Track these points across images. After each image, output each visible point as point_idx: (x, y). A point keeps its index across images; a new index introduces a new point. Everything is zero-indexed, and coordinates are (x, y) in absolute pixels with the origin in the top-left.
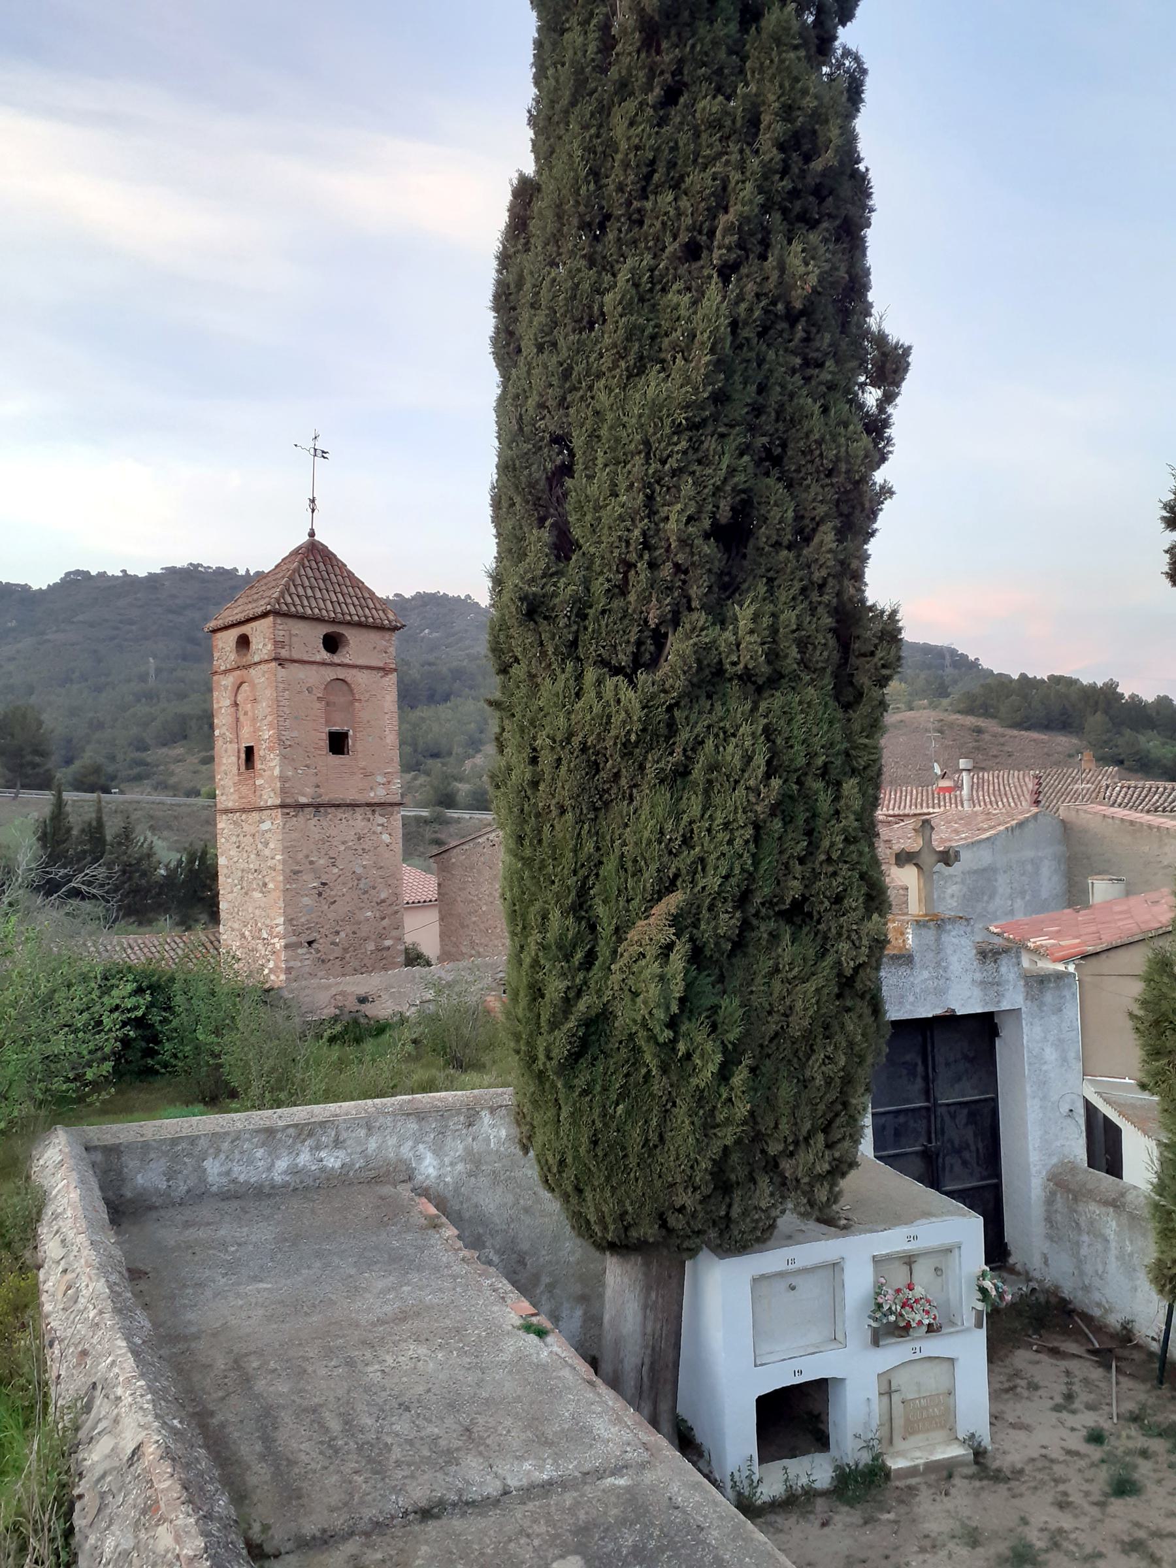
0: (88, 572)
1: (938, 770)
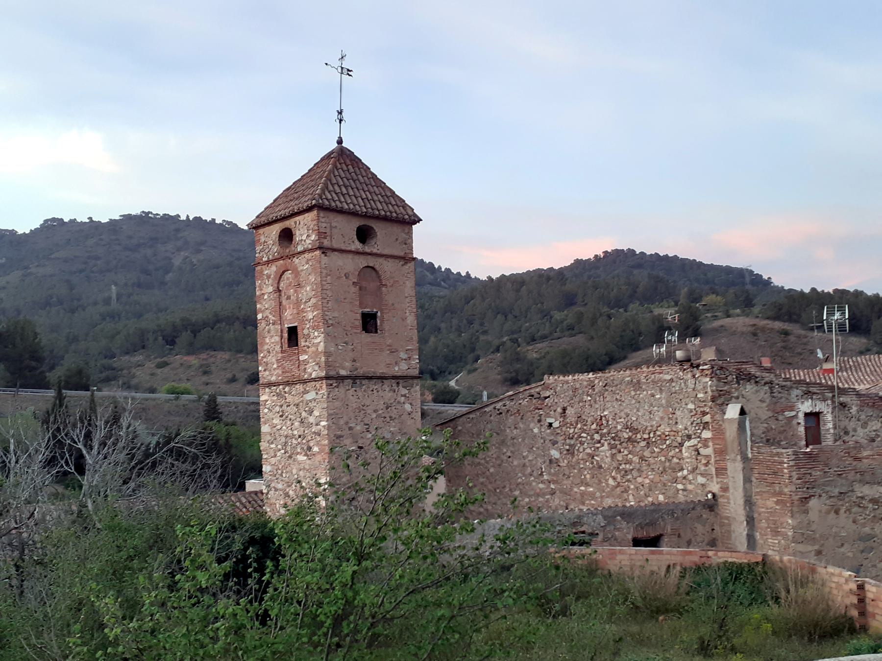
0: (62, 220)
1: (820, 355)
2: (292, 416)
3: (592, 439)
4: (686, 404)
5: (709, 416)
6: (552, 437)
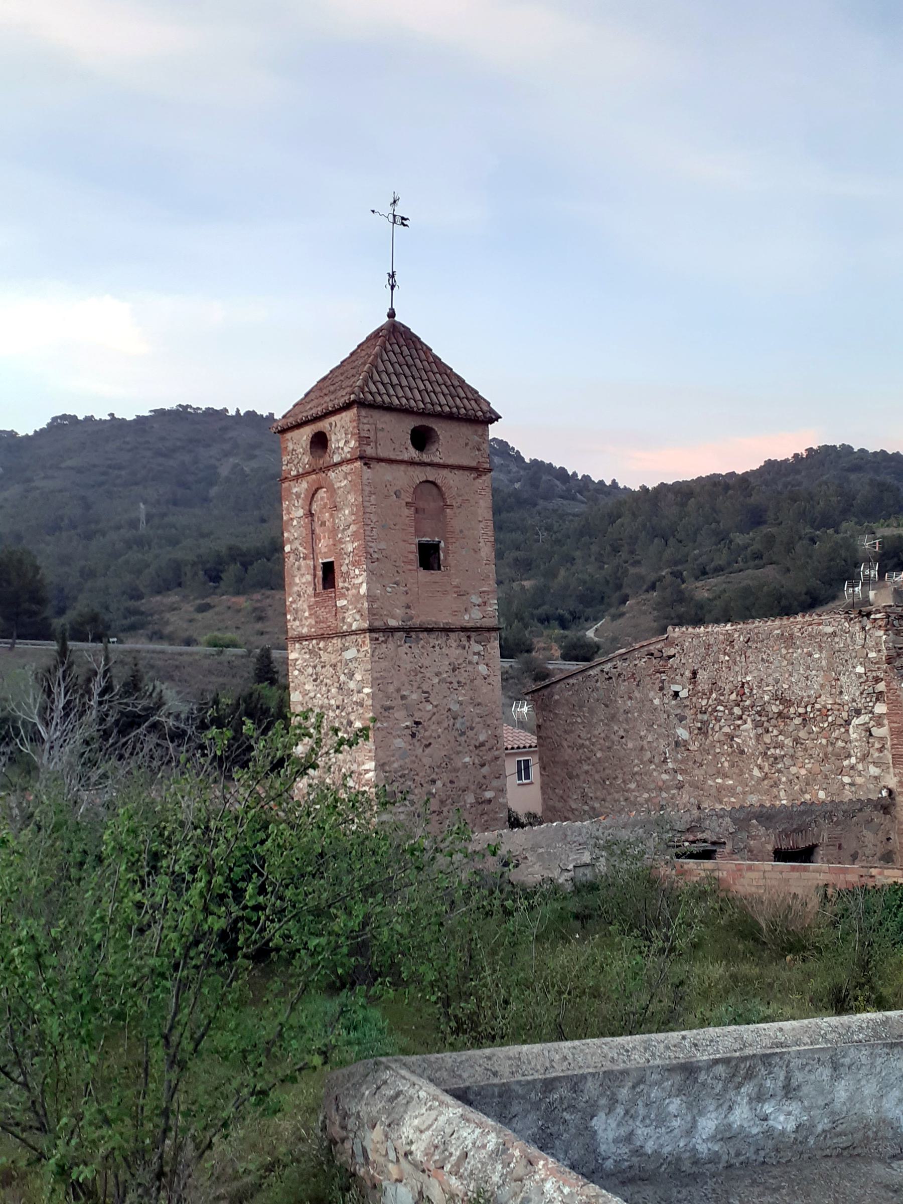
0: (75, 417)
2: (328, 681)
3: (731, 714)
4: (854, 667)
5: (883, 683)
6: (679, 711)
